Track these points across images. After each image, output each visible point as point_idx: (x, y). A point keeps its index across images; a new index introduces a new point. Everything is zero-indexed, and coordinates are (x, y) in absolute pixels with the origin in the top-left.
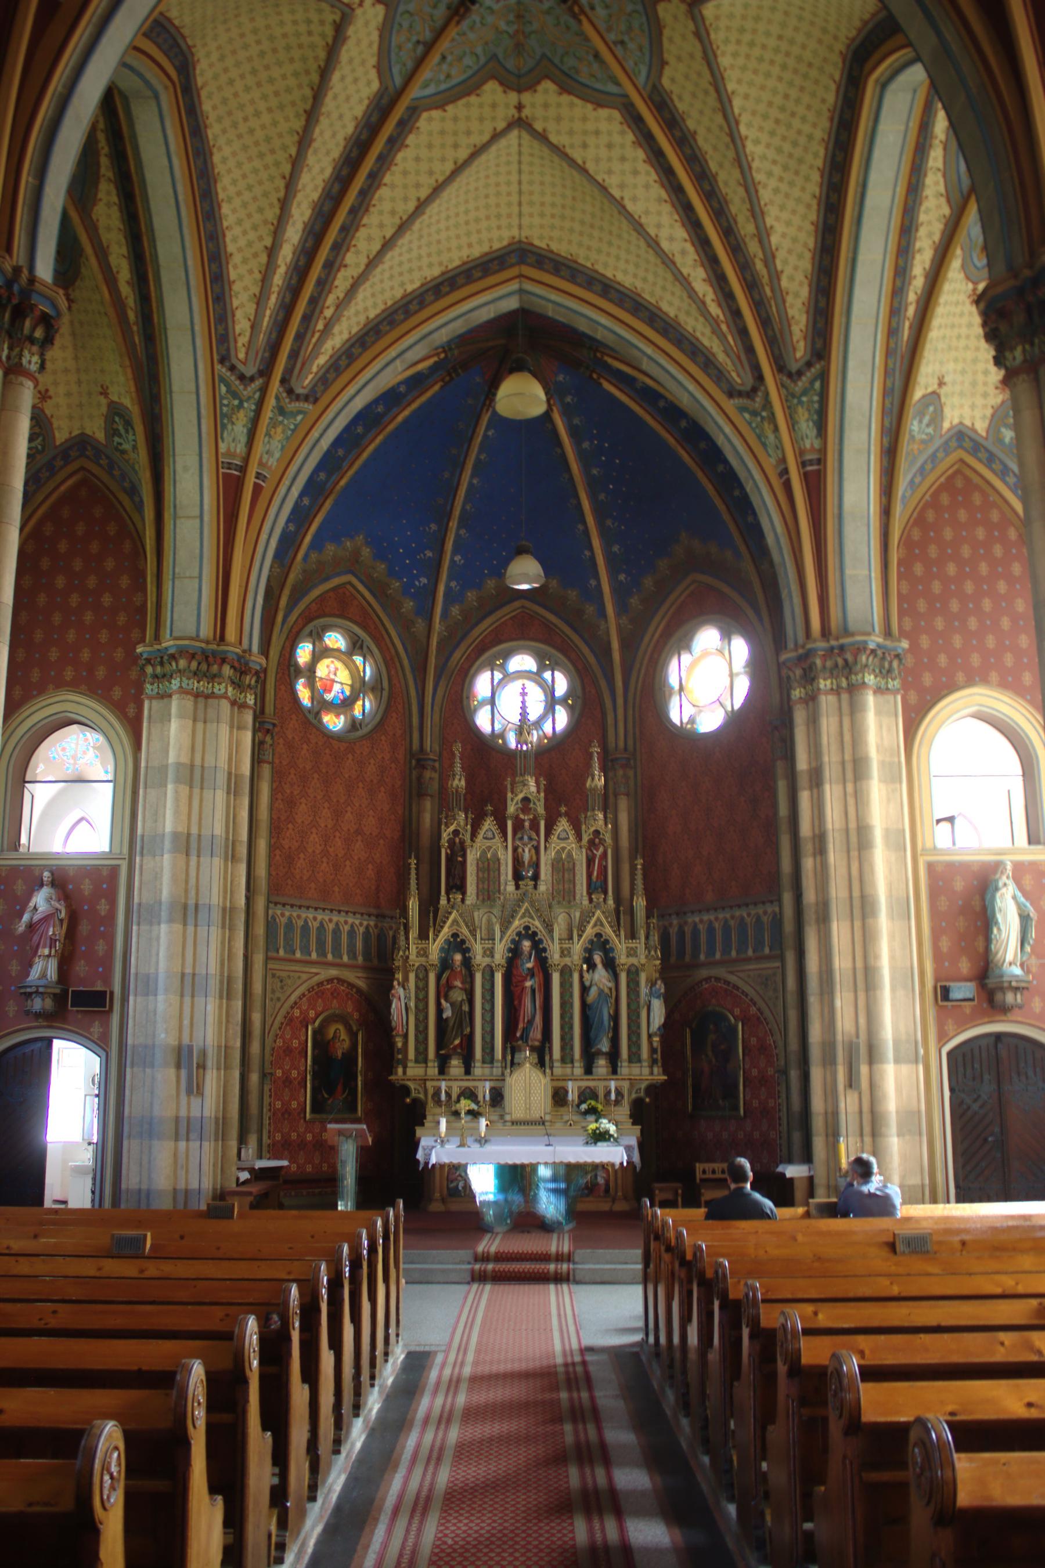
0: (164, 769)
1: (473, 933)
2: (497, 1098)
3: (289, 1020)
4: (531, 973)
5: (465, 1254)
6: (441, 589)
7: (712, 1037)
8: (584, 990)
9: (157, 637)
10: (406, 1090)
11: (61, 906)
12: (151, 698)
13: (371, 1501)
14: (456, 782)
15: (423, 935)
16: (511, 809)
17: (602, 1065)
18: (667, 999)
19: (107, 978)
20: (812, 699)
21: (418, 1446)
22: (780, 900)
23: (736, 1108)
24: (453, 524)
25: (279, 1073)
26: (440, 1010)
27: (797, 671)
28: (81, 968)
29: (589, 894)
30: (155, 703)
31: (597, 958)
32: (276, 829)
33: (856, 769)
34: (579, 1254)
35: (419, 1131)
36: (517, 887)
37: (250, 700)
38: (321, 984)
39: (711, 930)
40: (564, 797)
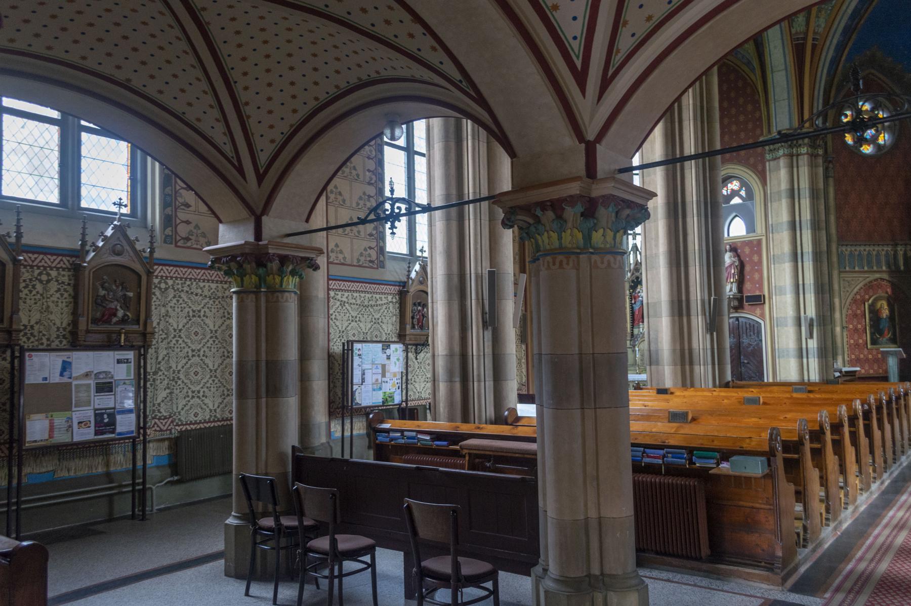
0: (779, 192)
3: (855, 301)
9: (769, 132)
11: (736, 259)
12: (769, 161)
19: (761, 288)
25: (851, 326)
28: (748, 286)
30: (772, 163)
32: (839, 208)
37: (821, 152)
38: (871, 282)
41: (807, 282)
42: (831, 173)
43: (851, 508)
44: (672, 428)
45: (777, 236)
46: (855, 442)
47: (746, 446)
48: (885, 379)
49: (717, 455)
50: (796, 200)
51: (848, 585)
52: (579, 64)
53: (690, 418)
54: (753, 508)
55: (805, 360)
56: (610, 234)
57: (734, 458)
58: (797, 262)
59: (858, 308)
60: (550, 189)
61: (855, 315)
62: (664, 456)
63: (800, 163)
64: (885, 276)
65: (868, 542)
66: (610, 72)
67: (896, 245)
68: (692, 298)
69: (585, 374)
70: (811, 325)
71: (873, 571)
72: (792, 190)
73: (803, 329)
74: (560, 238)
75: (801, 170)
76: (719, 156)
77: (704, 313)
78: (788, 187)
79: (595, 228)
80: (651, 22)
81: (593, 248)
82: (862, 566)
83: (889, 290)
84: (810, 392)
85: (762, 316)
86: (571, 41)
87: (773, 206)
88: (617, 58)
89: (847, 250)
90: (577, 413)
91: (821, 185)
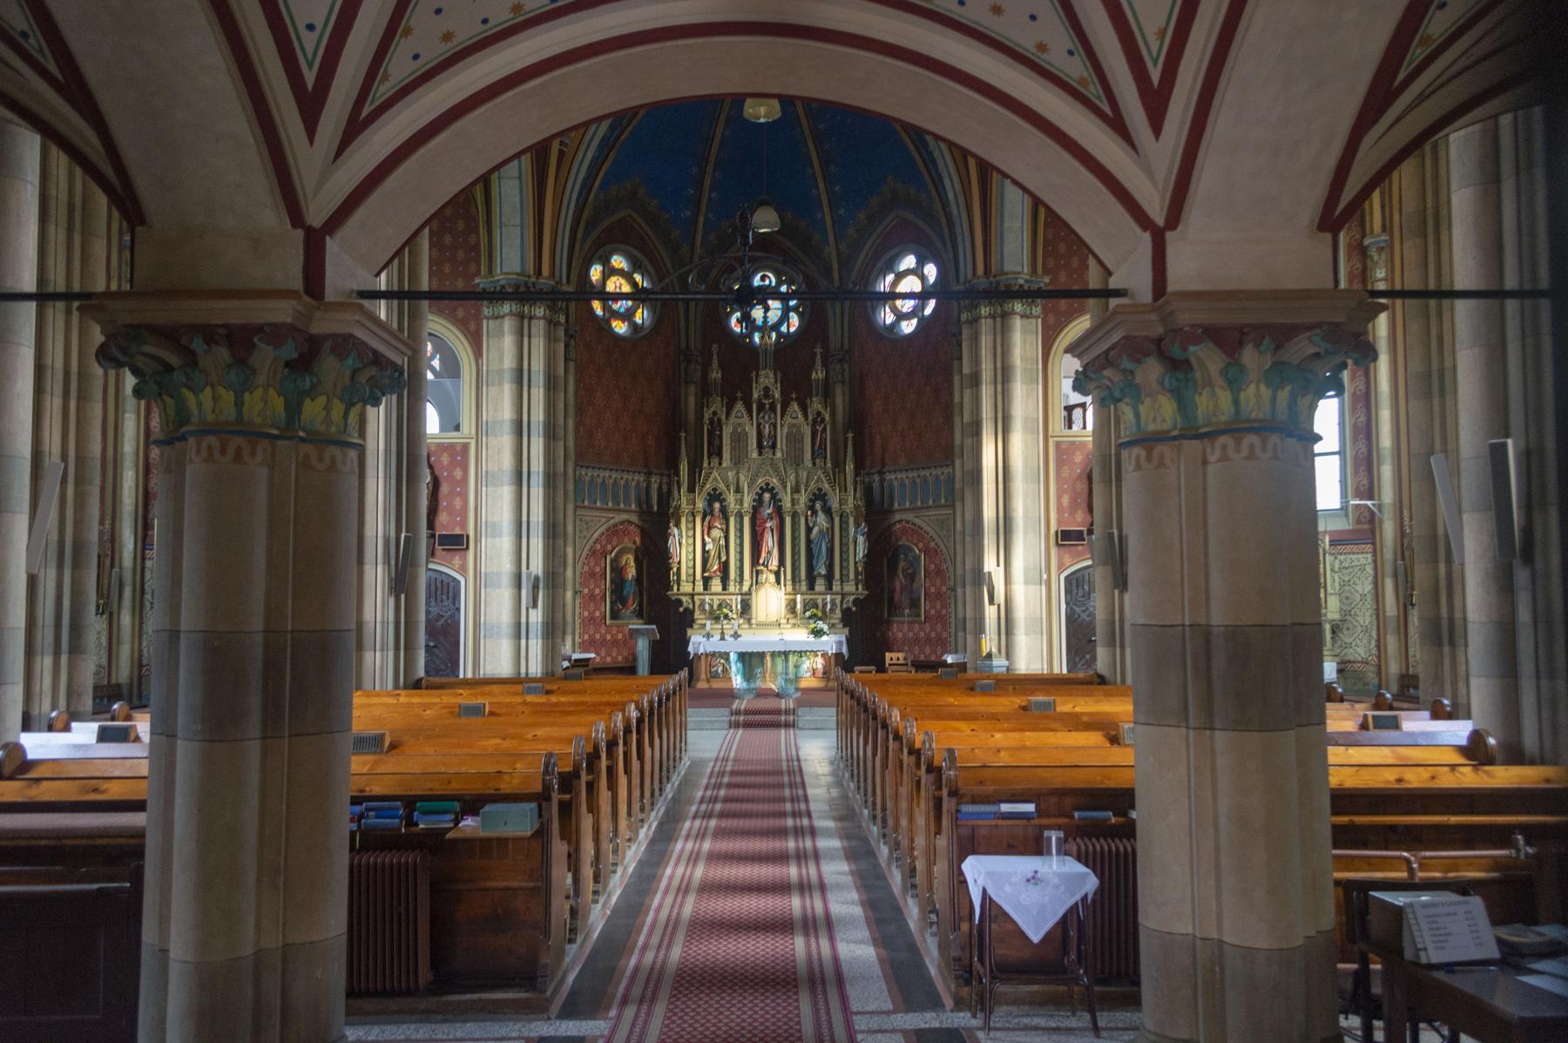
0: (500, 371)
1: (728, 487)
2: (746, 608)
3: (593, 552)
4: (771, 517)
5: (726, 711)
6: (701, 219)
7: (902, 564)
8: (809, 530)
9: (490, 271)
10: (680, 603)
13: (613, 969)
14: (714, 375)
15: (691, 490)
16: (756, 396)
17: (820, 586)
18: (869, 536)
19: (464, 524)
20: (975, 321)
21: (682, 850)
22: (953, 464)
23: (919, 615)
24: (710, 168)
26: (704, 544)
27: (972, 297)
28: (443, 518)
29: (813, 459)
31: (818, 506)
33: (1004, 376)
34: (801, 711)
35: (689, 632)
36: (760, 454)
37: (562, 319)
39: (902, 485)
40: (796, 387)
41: (533, 519)
42: (572, 355)
43: (620, 870)
44: (364, 764)
45: (493, 442)
46: (627, 771)
47: (505, 787)
48: (630, 669)
49: (456, 805)
50: (525, 388)
51: (637, 991)
52: (310, 77)
53: (387, 744)
54: (507, 889)
55: (523, 642)
56: (338, 408)
57: (488, 808)
58: (520, 485)
59: (597, 564)
60: (232, 304)
61: (592, 574)
62: (361, 816)
63: (534, 330)
64: (634, 518)
65: (649, 919)
66: (366, 111)
67: (649, 474)
68: (369, 532)
69: (263, 672)
70: (535, 587)
71: (664, 963)
72: (520, 371)
73: (524, 592)
74: (239, 403)
75: (534, 341)
76: (383, 302)
77: (387, 561)
78: (514, 365)
79: (312, 393)
80: (450, 45)
81: (304, 430)
82: (649, 957)
83: (638, 540)
84: (548, 692)
85: (463, 569)
86: (303, 32)
87: (490, 393)
88: (382, 89)
89: (587, 474)
90: (254, 748)
91: (561, 371)
